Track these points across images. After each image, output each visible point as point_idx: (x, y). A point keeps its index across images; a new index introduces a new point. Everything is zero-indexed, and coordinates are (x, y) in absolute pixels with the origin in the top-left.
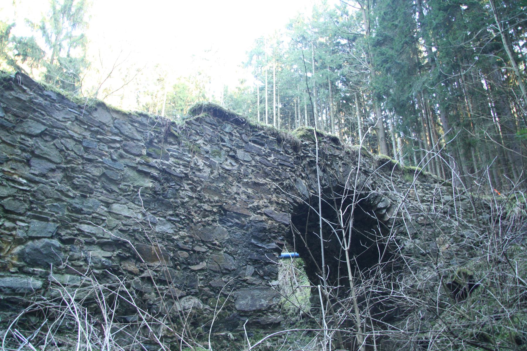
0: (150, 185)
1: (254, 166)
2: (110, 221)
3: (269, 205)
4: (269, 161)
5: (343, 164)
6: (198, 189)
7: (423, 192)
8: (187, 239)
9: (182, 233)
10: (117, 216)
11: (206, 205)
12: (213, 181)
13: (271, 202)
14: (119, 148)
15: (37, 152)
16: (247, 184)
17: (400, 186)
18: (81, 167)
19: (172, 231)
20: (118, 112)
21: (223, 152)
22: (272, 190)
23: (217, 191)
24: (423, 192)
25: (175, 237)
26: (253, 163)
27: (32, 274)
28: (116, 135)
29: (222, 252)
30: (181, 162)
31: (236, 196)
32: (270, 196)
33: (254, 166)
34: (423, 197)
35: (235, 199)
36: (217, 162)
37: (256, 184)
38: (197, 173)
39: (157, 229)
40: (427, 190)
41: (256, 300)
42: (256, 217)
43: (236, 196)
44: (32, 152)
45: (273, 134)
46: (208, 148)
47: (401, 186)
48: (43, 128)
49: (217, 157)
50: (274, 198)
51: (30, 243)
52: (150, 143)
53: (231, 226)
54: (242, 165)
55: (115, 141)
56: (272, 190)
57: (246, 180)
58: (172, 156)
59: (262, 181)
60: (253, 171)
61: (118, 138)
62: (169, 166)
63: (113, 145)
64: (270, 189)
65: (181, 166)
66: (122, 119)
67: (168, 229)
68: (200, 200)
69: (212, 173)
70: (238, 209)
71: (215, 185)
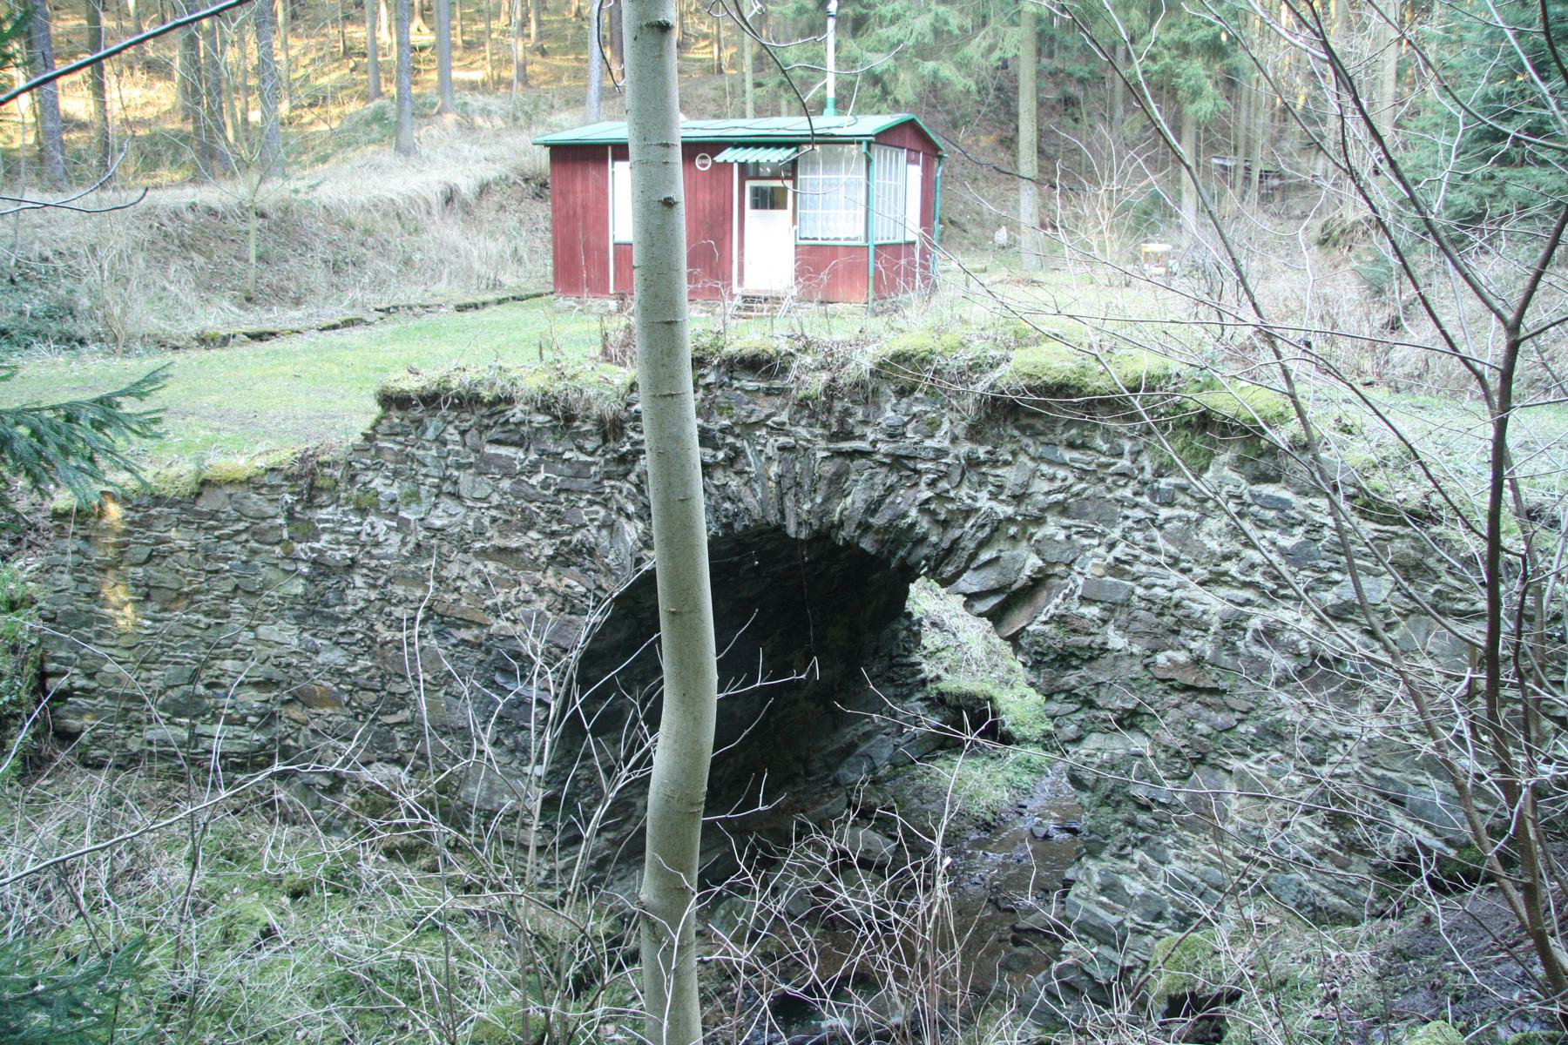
0: (300, 590)
1: (498, 507)
2: (259, 651)
3: (534, 597)
4: (533, 486)
5: (782, 449)
6: (381, 582)
7: (1236, 532)
8: (373, 671)
9: (361, 663)
10: (267, 643)
11: (401, 608)
12: (407, 561)
13: (538, 591)
14: (247, 541)
15: (152, 583)
16: (483, 554)
17: (1119, 493)
18: (205, 586)
19: (343, 661)
20: (232, 482)
21: (424, 490)
22: (543, 559)
23: (419, 580)
24: (1236, 532)
25: (350, 670)
26: (495, 499)
27: (180, 725)
28: (239, 520)
29: (441, 694)
30: (342, 538)
31: (459, 583)
32: (539, 575)
33: (498, 507)
34: (1226, 558)
35: (457, 589)
36: (412, 518)
37: (502, 553)
38: (375, 552)
39: (320, 659)
40: (1262, 524)
41: (495, 793)
42: (501, 628)
43: (459, 583)
44: (147, 585)
45: (545, 408)
46: (395, 490)
47: (1128, 492)
48: (148, 550)
49: (413, 506)
50: (549, 580)
51: (170, 692)
52: (290, 515)
53: (455, 646)
54: (472, 509)
55: (238, 532)
56: (543, 559)
57: (478, 545)
58: (324, 530)
59: (514, 542)
60: (494, 520)
61: (241, 526)
62: (321, 552)
63: (239, 539)
64: (537, 558)
65: (344, 547)
66: (239, 492)
67: (336, 657)
68: (386, 599)
69: (404, 543)
70: (463, 611)
71: (411, 567)
